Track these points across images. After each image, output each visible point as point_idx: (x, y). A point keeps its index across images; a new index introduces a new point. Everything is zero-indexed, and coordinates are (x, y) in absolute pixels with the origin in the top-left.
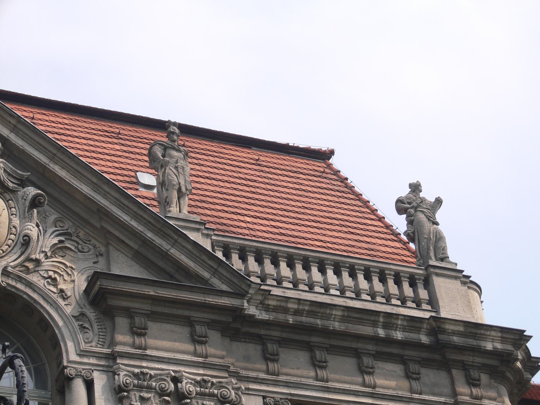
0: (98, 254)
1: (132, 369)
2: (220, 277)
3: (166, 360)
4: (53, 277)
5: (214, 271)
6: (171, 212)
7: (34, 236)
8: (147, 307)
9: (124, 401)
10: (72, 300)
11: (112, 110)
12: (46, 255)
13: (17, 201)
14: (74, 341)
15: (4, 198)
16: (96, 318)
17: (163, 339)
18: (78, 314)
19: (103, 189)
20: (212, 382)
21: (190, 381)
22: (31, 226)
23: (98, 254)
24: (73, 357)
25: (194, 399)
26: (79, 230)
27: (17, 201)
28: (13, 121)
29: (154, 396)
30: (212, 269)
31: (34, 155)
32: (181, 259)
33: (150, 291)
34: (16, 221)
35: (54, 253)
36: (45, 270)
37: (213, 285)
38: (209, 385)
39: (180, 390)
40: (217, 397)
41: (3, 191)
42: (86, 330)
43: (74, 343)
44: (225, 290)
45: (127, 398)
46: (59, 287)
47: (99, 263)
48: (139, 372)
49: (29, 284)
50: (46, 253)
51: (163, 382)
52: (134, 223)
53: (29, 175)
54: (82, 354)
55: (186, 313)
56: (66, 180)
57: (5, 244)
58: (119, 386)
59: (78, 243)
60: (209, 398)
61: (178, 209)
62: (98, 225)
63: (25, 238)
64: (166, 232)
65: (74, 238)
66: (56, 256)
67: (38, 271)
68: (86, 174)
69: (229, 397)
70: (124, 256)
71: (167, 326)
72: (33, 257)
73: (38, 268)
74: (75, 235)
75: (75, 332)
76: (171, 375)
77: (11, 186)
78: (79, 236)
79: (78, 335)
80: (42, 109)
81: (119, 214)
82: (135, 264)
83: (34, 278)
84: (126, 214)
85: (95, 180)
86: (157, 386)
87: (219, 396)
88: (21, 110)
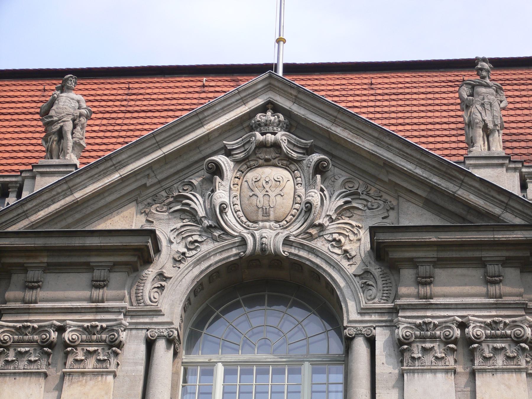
0: (389, 208)
1: (414, 320)
2: (513, 211)
3: (453, 306)
4: (337, 239)
5: (505, 205)
6: (472, 151)
7: (316, 201)
8: (432, 254)
9: (405, 354)
10: (358, 260)
11: (37, 68)
12: (331, 218)
13: (303, 170)
14: (355, 301)
15: (290, 170)
16: (381, 273)
17: (453, 285)
18: (362, 273)
19: (385, 142)
20: (505, 322)
21: (478, 324)
22: (313, 192)
23: (389, 208)
24: (354, 315)
25: (484, 343)
26: (370, 187)
27: (303, 170)
28: (294, 92)
29: (439, 345)
30: (503, 204)
31: (316, 122)
32: (470, 199)
33: (430, 237)
34: (301, 190)
35: (340, 215)
36: (330, 234)
37: (505, 220)
38: (502, 325)
39: (467, 335)
40: (511, 337)
41: (288, 163)
42: (370, 287)
43: (356, 303)
44: (518, 223)
45: (408, 351)
46: (343, 248)
47: (389, 217)
48: (421, 322)
49: (312, 251)
50: (330, 217)
51: (447, 330)
52: (419, 171)
53: (312, 142)
54: (363, 312)
55: (477, 254)
56: (348, 140)
57: (290, 215)
58: (399, 340)
59: (367, 201)
60: (501, 339)
61: (486, 147)
62: (386, 179)
63: (307, 205)
64: (452, 173)
65: (364, 197)
66: (343, 217)
67: (323, 235)
68: (367, 130)
69: (523, 336)
70: (415, 205)
71: (459, 271)
72: (317, 222)
73: (322, 233)
74: (365, 193)
75: (356, 291)
76: (457, 321)
77: (296, 156)
78: (369, 194)
79: (359, 293)
80: (11, 81)
81: (403, 164)
82: (426, 212)
83: (320, 245)
84: (411, 163)
85: (376, 134)
86: (442, 334)
87: (512, 336)
88: (361, 78)
